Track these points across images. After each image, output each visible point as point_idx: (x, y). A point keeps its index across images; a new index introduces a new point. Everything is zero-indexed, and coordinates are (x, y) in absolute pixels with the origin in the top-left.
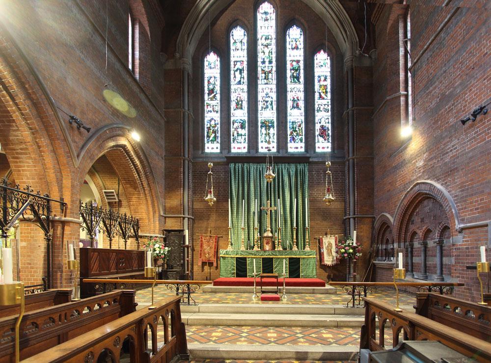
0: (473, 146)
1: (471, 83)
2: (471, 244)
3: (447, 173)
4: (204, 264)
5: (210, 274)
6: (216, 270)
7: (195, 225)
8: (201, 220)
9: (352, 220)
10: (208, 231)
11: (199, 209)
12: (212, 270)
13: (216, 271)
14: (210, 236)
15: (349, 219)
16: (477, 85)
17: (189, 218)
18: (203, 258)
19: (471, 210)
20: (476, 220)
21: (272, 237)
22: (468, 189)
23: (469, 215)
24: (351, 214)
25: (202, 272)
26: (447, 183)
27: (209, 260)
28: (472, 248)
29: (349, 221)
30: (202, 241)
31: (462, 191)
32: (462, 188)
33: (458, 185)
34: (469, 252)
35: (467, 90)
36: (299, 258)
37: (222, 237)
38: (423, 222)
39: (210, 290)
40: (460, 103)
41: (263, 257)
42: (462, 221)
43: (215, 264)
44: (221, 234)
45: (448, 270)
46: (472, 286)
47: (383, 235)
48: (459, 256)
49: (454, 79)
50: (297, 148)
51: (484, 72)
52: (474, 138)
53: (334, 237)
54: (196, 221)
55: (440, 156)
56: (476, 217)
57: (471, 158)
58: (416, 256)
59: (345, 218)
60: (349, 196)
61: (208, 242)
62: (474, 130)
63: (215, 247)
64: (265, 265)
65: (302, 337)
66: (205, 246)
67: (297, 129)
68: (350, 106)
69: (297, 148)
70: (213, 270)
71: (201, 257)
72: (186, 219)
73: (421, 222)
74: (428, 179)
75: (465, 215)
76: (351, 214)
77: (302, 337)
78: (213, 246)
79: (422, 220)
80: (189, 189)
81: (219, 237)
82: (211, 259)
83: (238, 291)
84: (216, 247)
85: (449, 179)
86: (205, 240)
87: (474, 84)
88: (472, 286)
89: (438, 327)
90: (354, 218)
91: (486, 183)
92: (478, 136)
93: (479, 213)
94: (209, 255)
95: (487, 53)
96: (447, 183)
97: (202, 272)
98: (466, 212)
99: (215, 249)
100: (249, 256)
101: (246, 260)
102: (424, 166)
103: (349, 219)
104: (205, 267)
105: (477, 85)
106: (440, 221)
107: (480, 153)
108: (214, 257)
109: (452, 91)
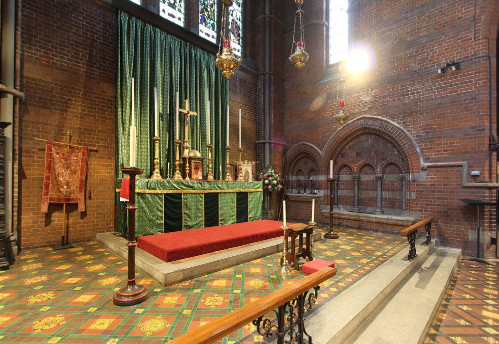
0: (442, 94)
1: (441, 38)
2: (438, 181)
3: (408, 113)
4: (54, 207)
5: (68, 227)
6: (82, 218)
7: (26, 117)
8: (44, 107)
9: (267, 145)
10: (65, 135)
11: (40, 80)
12: (71, 221)
13: (82, 221)
14: (70, 147)
15: (264, 143)
16: (448, 42)
17: (15, 97)
18: (53, 194)
19: (438, 151)
20: (445, 160)
21: (202, 160)
22: (435, 132)
23: (435, 155)
24: (267, 138)
25: (46, 225)
26: (406, 122)
27: (69, 199)
28: (438, 185)
29: (264, 146)
30: (50, 155)
31: (426, 132)
32: (427, 129)
33: (421, 127)
34: (435, 188)
35: (435, 43)
36: (218, 193)
37: (96, 151)
38: (360, 156)
39: (181, 277)
40: (426, 52)
41: (206, 192)
42: (427, 160)
43: (81, 207)
44: (95, 146)
45: (388, 203)
46: (438, 218)
47: (294, 166)
48: (422, 191)
49: (419, 29)
50: (208, 35)
51: (458, 32)
52: (444, 87)
53: (250, 165)
54: (30, 108)
55: (397, 96)
56: (445, 158)
57: (438, 105)
58: (342, 189)
59: (257, 142)
60: (265, 116)
61: (66, 160)
62: (444, 80)
63: (82, 170)
64: (317, 213)
65: (487, 325)
66: (59, 168)
67: (209, 10)
68: (267, 12)
69: (208, 35)
70: (74, 218)
71: (47, 194)
72: (10, 97)
73: (357, 156)
74: (378, 115)
75: (431, 155)
76: (267, 138)
77: (487, 325)
78: (78, 169)
79: (358, 154)
80: (16, 25)
81: (91, 151)
82: (73, 196)
83: (229, 263)
84: (85, 170)
85: (409, 119)
86: (57, 153)
87: (445, 40)
88: (438, 218)
89: (253, 247)
90: (270, 144)
91: (458, 129)
92: (448, 86)
93: (448, 154)
94: (68, 188)
95: (462, 17)
96: (406, 122)
97: (46, 225)
98: (433, 151)
99: (81, 174)
100: (186, 191)
101: (181, 199)
102: (372, 102)
103: (264, 143)
104: (56, 214)
105: (448, 42)
106: (384, 157)
107: (451, 102)
108: (80, 191)
109: (416, 39)
